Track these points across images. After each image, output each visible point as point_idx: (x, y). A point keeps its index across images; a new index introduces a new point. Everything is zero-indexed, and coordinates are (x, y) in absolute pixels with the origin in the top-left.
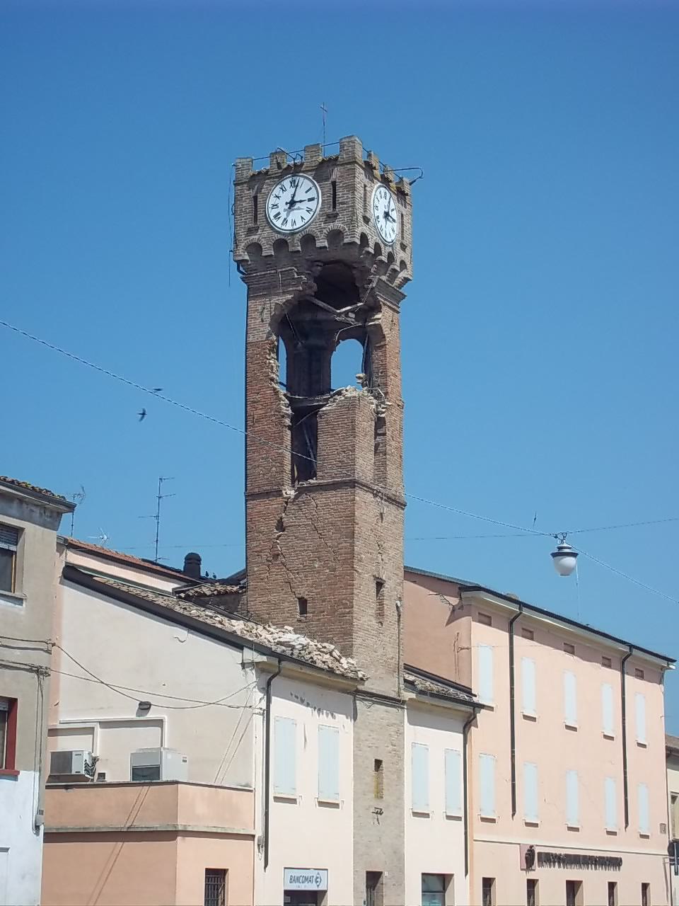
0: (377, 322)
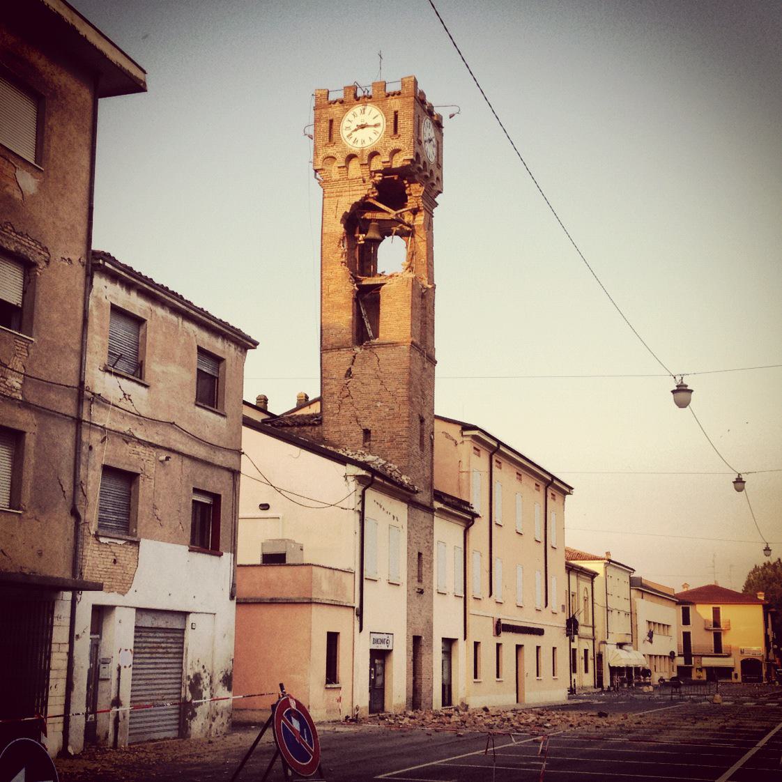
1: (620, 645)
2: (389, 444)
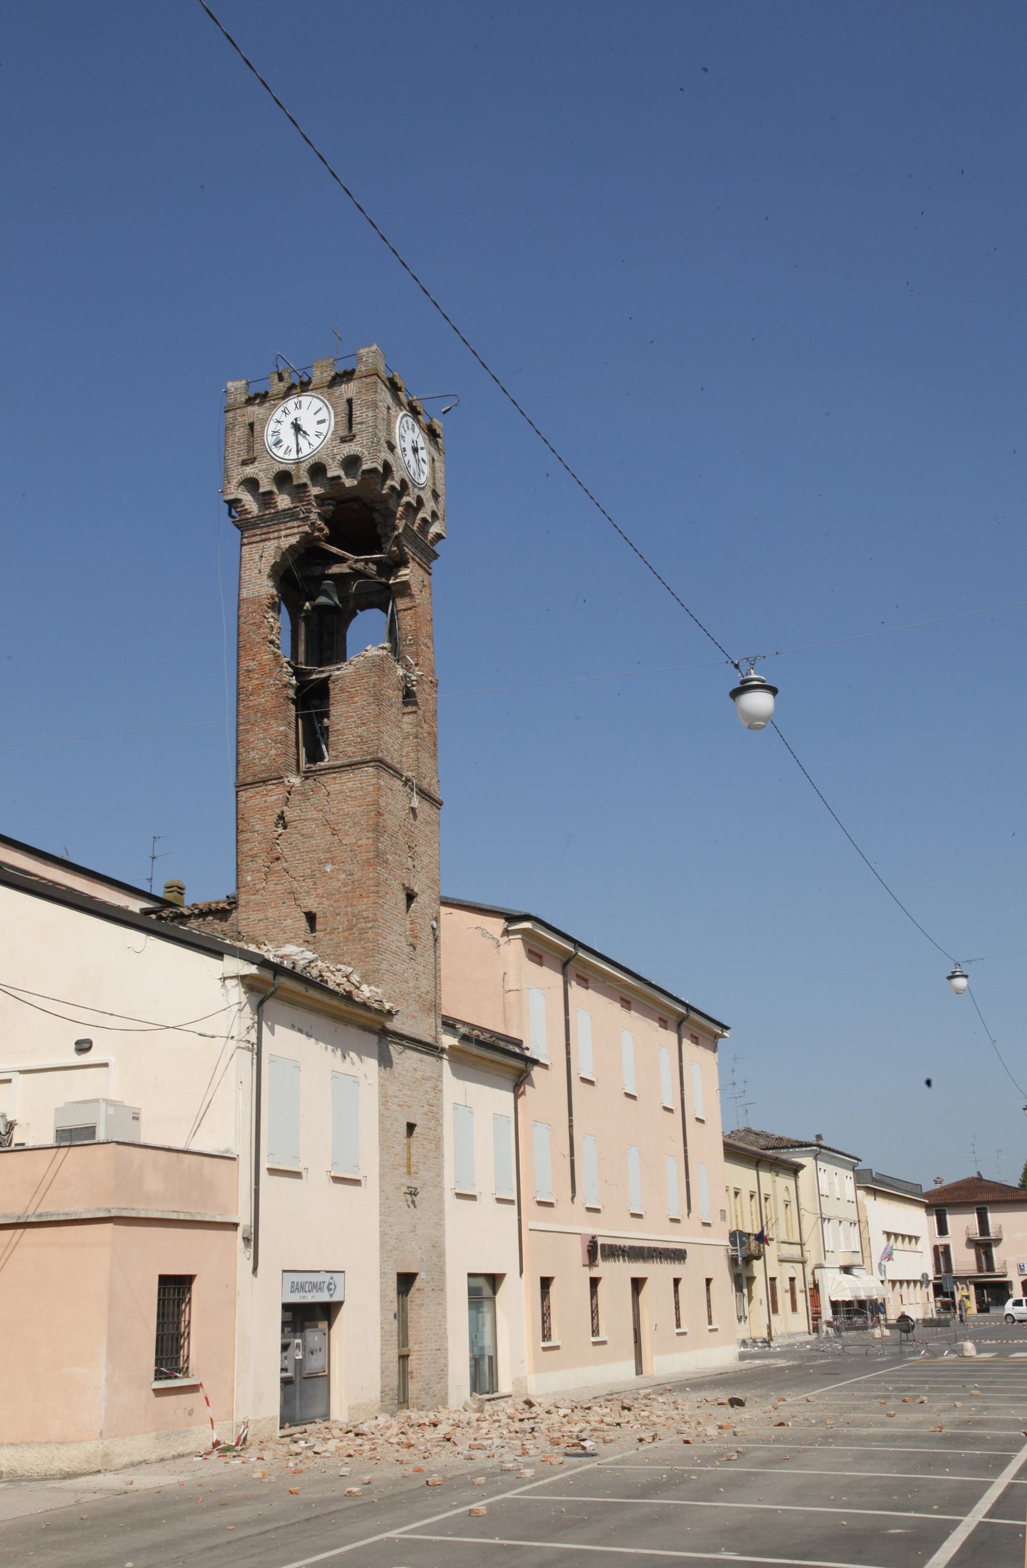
0: (404, 579)
1: (847, 1270)
2: (346, 934)
